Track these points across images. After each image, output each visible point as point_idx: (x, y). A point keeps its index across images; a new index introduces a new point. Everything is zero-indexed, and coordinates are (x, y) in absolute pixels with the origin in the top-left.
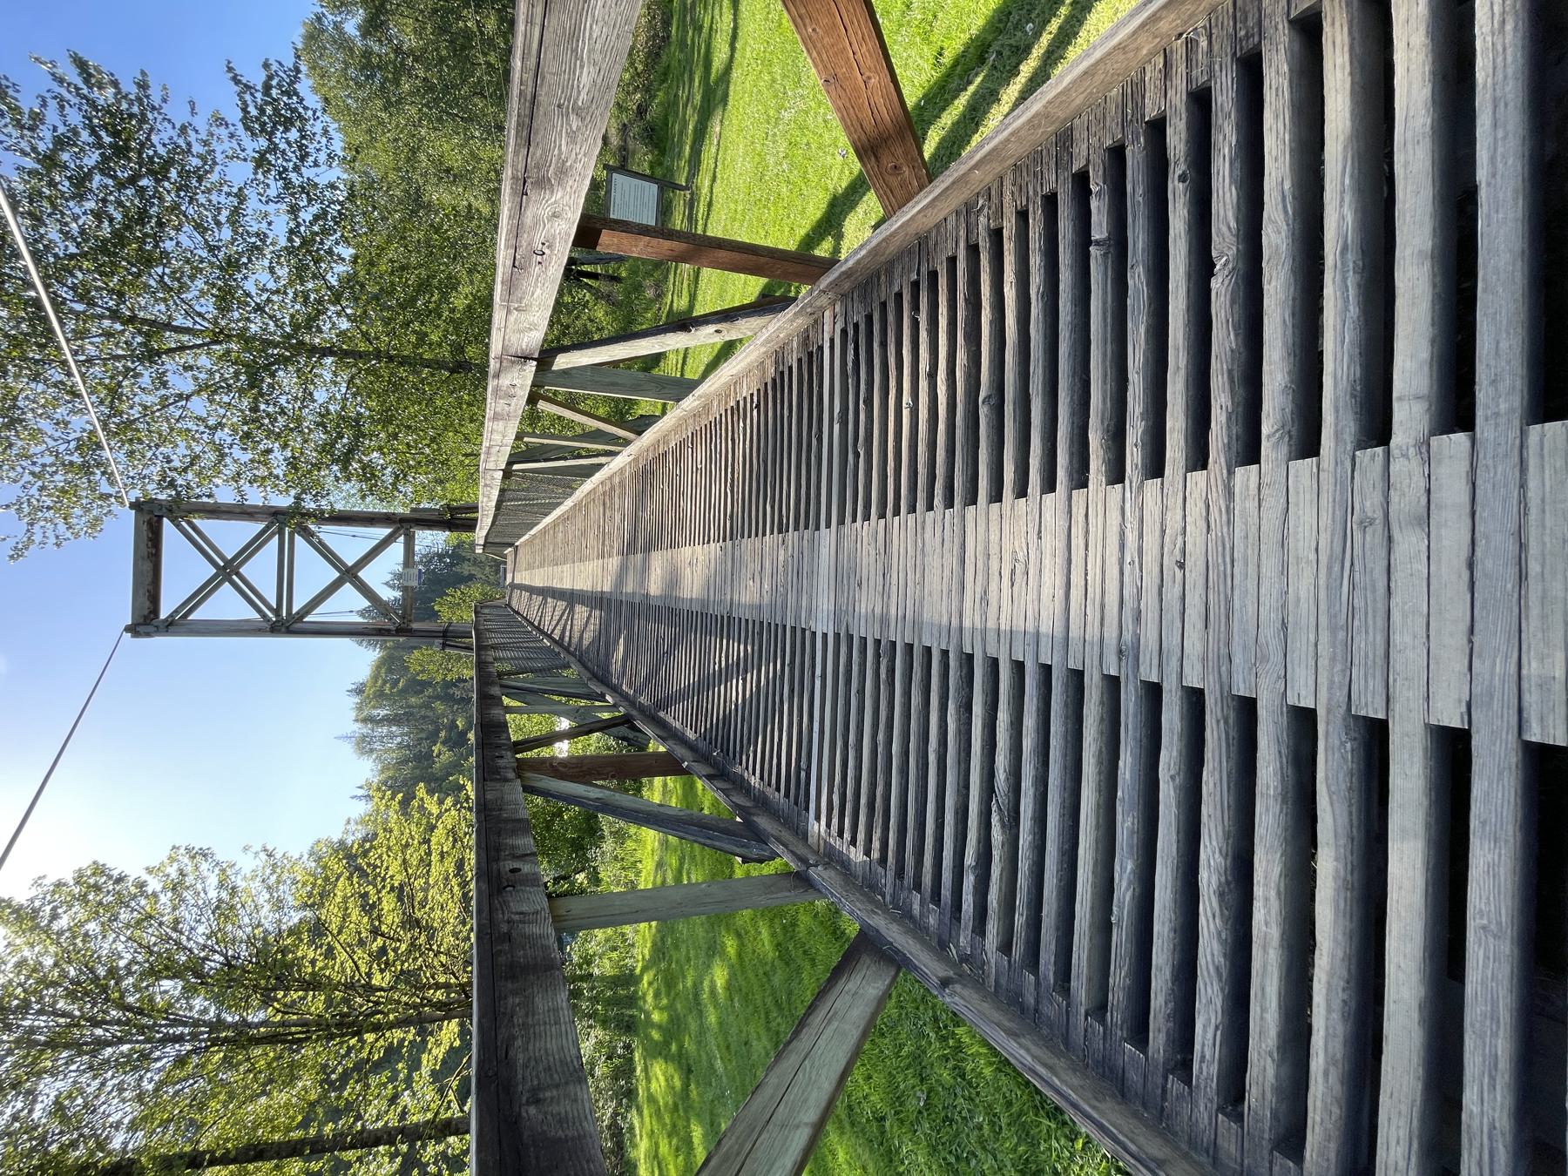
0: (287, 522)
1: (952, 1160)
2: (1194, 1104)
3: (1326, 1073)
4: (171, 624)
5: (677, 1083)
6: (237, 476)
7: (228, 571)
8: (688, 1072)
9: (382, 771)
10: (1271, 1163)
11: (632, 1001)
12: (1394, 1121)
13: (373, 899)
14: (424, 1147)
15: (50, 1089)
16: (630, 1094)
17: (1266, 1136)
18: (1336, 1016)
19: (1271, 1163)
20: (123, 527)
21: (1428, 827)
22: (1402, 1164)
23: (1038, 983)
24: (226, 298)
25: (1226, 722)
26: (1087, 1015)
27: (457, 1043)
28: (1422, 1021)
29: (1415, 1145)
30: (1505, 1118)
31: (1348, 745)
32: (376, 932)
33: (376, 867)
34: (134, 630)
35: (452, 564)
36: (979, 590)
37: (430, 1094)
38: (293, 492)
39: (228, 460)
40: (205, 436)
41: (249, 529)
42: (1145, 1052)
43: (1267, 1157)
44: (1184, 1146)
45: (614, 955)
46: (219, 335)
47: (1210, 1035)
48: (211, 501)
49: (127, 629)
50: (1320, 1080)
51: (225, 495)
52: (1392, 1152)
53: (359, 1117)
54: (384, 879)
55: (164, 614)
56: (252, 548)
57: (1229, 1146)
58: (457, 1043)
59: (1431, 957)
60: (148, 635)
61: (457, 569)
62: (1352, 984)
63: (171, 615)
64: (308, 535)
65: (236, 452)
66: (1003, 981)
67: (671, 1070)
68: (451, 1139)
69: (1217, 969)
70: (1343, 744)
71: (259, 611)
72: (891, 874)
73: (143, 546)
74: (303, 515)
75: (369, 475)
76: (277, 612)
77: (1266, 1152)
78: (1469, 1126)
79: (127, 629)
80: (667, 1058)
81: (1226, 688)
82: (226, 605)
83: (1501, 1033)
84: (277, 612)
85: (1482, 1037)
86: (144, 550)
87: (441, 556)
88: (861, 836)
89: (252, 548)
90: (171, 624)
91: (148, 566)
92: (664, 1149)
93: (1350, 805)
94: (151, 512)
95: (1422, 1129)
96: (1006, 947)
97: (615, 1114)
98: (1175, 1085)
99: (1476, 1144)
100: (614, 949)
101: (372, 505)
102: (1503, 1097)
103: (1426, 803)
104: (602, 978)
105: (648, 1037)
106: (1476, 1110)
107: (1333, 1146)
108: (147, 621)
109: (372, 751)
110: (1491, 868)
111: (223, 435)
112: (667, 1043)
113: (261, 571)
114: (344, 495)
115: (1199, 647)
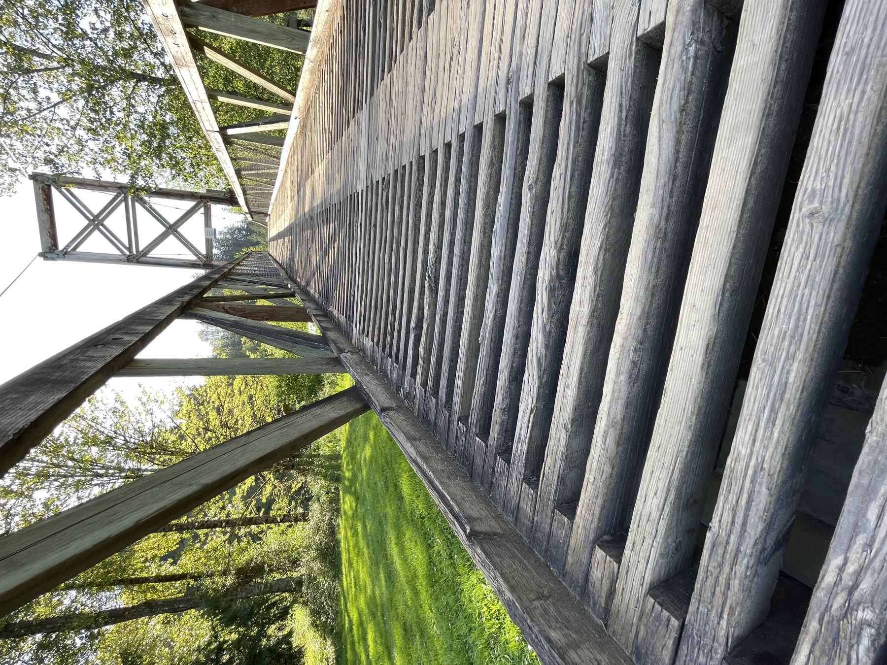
0: (130, 193)
1: (450, 537)
2: (509, 476)
3: (605, 437)
4: (66, 253)
5: (354, 505)
6: (94, 162)
7: (96, 222)
8: (357, 499)
9: (214, 350)
10: (552, 518)
11: (339, 467)
12: (656, 474)
13: (203, 412)
14: (239, 530)
15: (40, 495)
16: (338, 510)
17: (552, 497)
18: (623, 378)
19: (552, 518)
20: (27, 190)
21: (767, 114)
22: (655, 515)
23: (437, 403)
24: (70, 31)
25: (579, 103)
26: (459, 419)
27: (254, 484)
28: (707, 365)
29: (672, 496)
30: (778, 457)
31: (692, 49)
32: (207, 429)
33: (202, 396)
34: (44, 255)
35: (247, 235)
36: (431, 92)
37: (241, 505)
38: (129, 172)
39: (87, 150)
40: (69, 132)
41: (106, 197)
42: (486, 442)
43: (549, 514)
44: (500, 510)
45: (330, 445)
46: (67, 62)
47: (526, 419)
48: (80, 177)
49: (40, 255)
50: (599, 443)
51: (88, 174)
52: (648, 503)
53: (206, 515)
54: (209, 403)
55: (61, 246)
56: (109, 209)
57: (526, 507)
58: (254, 484)
59: (734, 291)
60: (53, 259)
61: (249, 238)
62: (647, 345)
63: (65, 248)
64: (143, 203)
65: (91, 144)
66: (421, 408)
67: (352, 499)
68: (253, 527)
69: (539, 360)
70: (685, 48)
71: (119, 249)
72: (380, 349)
73: (42, 204)
74: (138, 190)
75: (176, 165)
76: (130, 249)
77: (549, 511)
78: (732, 471)
79: (40, 255)
80: (351, 493)
81: (583, 59)
82: (96, 243)
83: (800, 355)
84: (130, 249)
85: (772, 364)
86: (43, 207)
87: (240, 230)
88: (370, 333)
89: (109, 209)
90: (66, 253)
91: (46, 217)
92: (349, 534)
93: (679, 132)
94: (43, 182)
95: (683, 481)
96: (424, 385)
97: (331, 519)
98: (500, 464)
99: (736, 489)
100: (331, 442)
101: (179, 185)
102: (782, 432)
103: (770, 76)
104: (324, 456)
105: (344, 484)
106: (744, 451)
107: (599, 502)
108: (51, 249)
109: (207, 339)
110: (844, 124)
111: (80, 132)
112: (351, 486)
113: (116, 222)
114: (163, 179)
115: (566, 24)
